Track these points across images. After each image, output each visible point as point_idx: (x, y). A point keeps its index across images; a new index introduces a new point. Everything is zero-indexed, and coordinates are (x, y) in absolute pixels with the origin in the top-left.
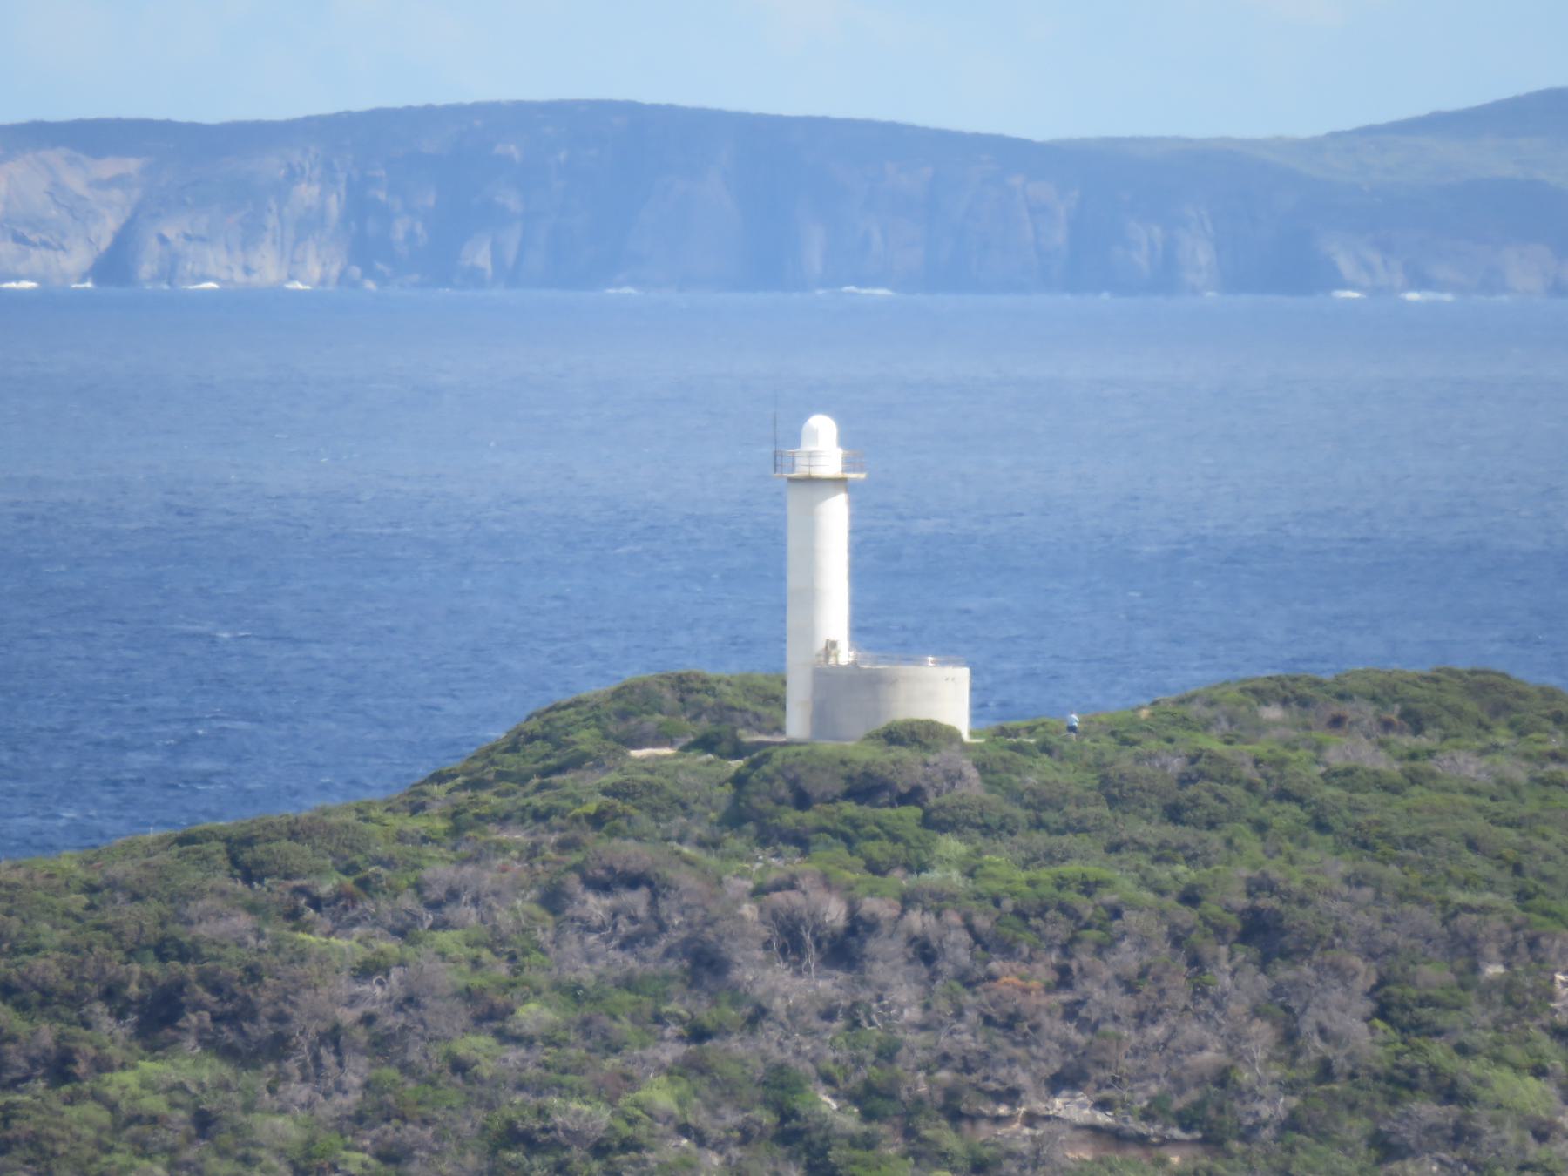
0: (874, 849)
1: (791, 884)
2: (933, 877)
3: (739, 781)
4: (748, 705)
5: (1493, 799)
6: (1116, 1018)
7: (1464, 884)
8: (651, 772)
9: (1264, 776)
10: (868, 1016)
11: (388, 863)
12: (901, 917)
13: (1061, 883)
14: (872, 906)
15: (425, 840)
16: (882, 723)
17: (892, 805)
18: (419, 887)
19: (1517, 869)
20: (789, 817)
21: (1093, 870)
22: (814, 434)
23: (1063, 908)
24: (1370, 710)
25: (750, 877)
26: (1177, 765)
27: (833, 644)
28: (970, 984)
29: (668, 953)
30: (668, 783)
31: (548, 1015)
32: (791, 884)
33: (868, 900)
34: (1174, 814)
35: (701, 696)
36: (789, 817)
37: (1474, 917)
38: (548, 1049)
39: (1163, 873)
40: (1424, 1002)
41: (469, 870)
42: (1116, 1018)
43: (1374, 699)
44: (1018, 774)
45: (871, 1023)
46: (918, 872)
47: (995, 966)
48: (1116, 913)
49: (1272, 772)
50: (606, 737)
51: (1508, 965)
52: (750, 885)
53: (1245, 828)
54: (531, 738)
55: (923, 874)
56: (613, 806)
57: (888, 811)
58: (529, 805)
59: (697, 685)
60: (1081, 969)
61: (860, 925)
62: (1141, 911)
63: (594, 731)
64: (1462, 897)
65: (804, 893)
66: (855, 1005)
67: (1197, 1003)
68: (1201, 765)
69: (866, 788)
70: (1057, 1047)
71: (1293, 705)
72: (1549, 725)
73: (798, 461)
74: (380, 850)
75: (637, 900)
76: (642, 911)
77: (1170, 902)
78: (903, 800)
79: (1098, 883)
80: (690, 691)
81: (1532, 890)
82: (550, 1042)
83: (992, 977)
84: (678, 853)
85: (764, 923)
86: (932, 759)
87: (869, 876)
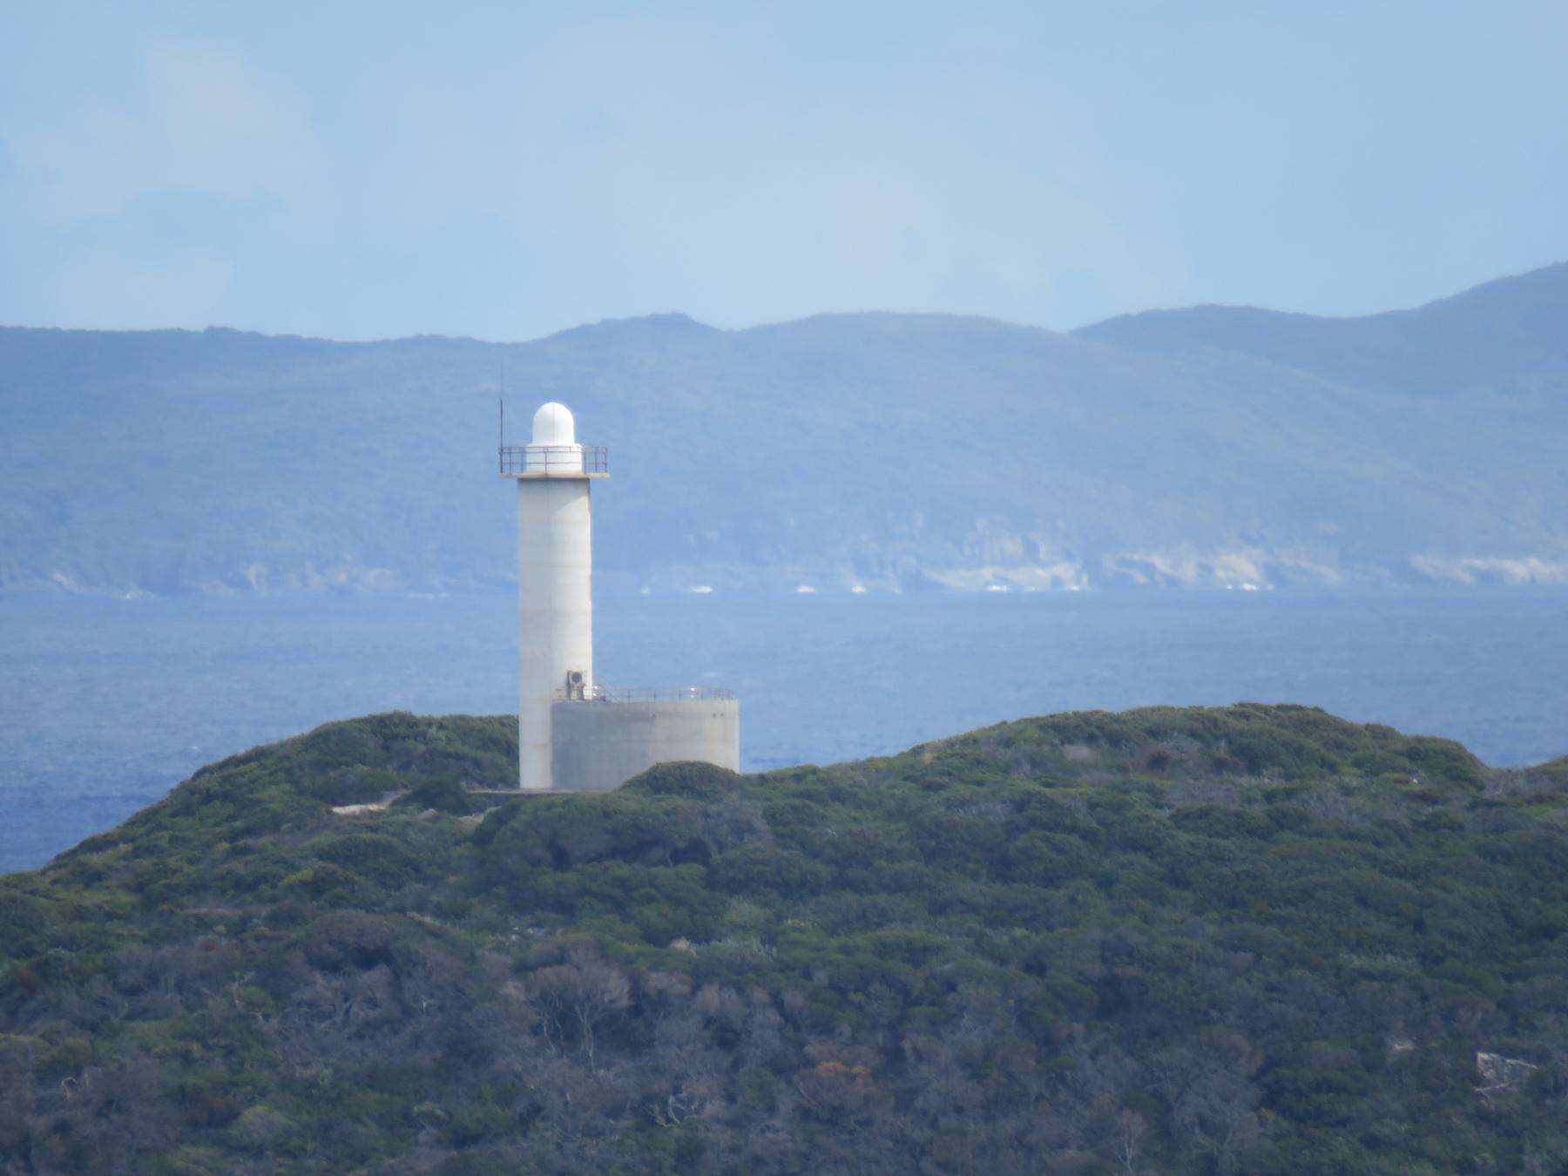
0: (650, 913)
1: (561, 958)
2: (729, 945)
3: (481, 838)
4: (465, 750)
5: (1377, 844)
6: (959, 1110)
7: (1356, 947)
8: (374, 829)
9: (1102, 822)
10: (664, 1112)
11: (70, 943)
12: (693, 993)
13: (884, 950)
14: (657, 981)
15: (109, 916)
16: (639, 768)
17: (665, 863)
18: (110, 971)
19: (1419, 926)
20: (548, 879)
21: (918, 933)
22: (551, 426)
23: (886, 979)
24: (1194, 747)
25: (508, 952)
26: (1000, 812)
27: (577, 677)
28: (780, 1068)
29: (417, 1041)
30: (395, 841)
31: (280, 1119)
32: (561, 958)
33: (654, 975)
34: (1003, 868)
35: (410, 743)
36: (548, 879)
37: (1376, 985)
38: (281, 1160)
39: (1001, 938)
40: (1319, 1087)
41: (167, 950)
42: (959, 1110)
43: (1193, 735)
44: (813, 825)
45: (669, 1120)
46: (708, 941)
47: (812, 1050)
48: (951, 987)
49: (1112, 817)
50: (301, 792)
51: (1419, 1042)
52: (510, 961)
53: (1088, 884)
54: (208, 798)
55: (714, 943)
56: (334, 873)
57: (661, 870)
58: (229, 872)
59: (402, 730)
60: (915, 1049)
61: (645, 1005)
62: (979, 982)
63: (287, 787)
64: (1358, 961)
65: (579, 968)
66: (648, 1098)
67: (1055, 1091)
68: (1029, 812)
69: (634, 841)
70: (890, 1144)
71: (1102, 742)
72: (1406, 763)
73: (529, 458)
74: (58, 929)
75: (376, 978)
76: (380, 995)
77: (1012, 970)
78: (678, 857)
79: (926, 950)
80: (395, 737)
81: (1440, 952)
82: (283, 1150)
83: (809, 1063)
84: (421, 924)
85: (533, 1003)
86: (714, 808)
87: (651, 948)
